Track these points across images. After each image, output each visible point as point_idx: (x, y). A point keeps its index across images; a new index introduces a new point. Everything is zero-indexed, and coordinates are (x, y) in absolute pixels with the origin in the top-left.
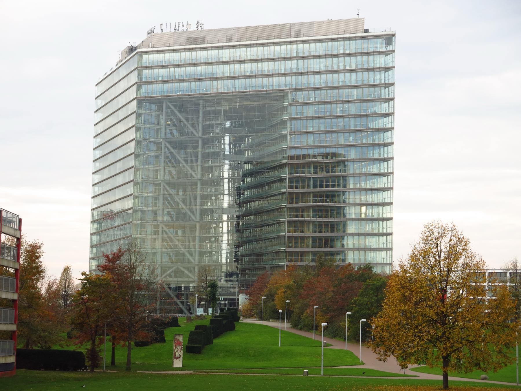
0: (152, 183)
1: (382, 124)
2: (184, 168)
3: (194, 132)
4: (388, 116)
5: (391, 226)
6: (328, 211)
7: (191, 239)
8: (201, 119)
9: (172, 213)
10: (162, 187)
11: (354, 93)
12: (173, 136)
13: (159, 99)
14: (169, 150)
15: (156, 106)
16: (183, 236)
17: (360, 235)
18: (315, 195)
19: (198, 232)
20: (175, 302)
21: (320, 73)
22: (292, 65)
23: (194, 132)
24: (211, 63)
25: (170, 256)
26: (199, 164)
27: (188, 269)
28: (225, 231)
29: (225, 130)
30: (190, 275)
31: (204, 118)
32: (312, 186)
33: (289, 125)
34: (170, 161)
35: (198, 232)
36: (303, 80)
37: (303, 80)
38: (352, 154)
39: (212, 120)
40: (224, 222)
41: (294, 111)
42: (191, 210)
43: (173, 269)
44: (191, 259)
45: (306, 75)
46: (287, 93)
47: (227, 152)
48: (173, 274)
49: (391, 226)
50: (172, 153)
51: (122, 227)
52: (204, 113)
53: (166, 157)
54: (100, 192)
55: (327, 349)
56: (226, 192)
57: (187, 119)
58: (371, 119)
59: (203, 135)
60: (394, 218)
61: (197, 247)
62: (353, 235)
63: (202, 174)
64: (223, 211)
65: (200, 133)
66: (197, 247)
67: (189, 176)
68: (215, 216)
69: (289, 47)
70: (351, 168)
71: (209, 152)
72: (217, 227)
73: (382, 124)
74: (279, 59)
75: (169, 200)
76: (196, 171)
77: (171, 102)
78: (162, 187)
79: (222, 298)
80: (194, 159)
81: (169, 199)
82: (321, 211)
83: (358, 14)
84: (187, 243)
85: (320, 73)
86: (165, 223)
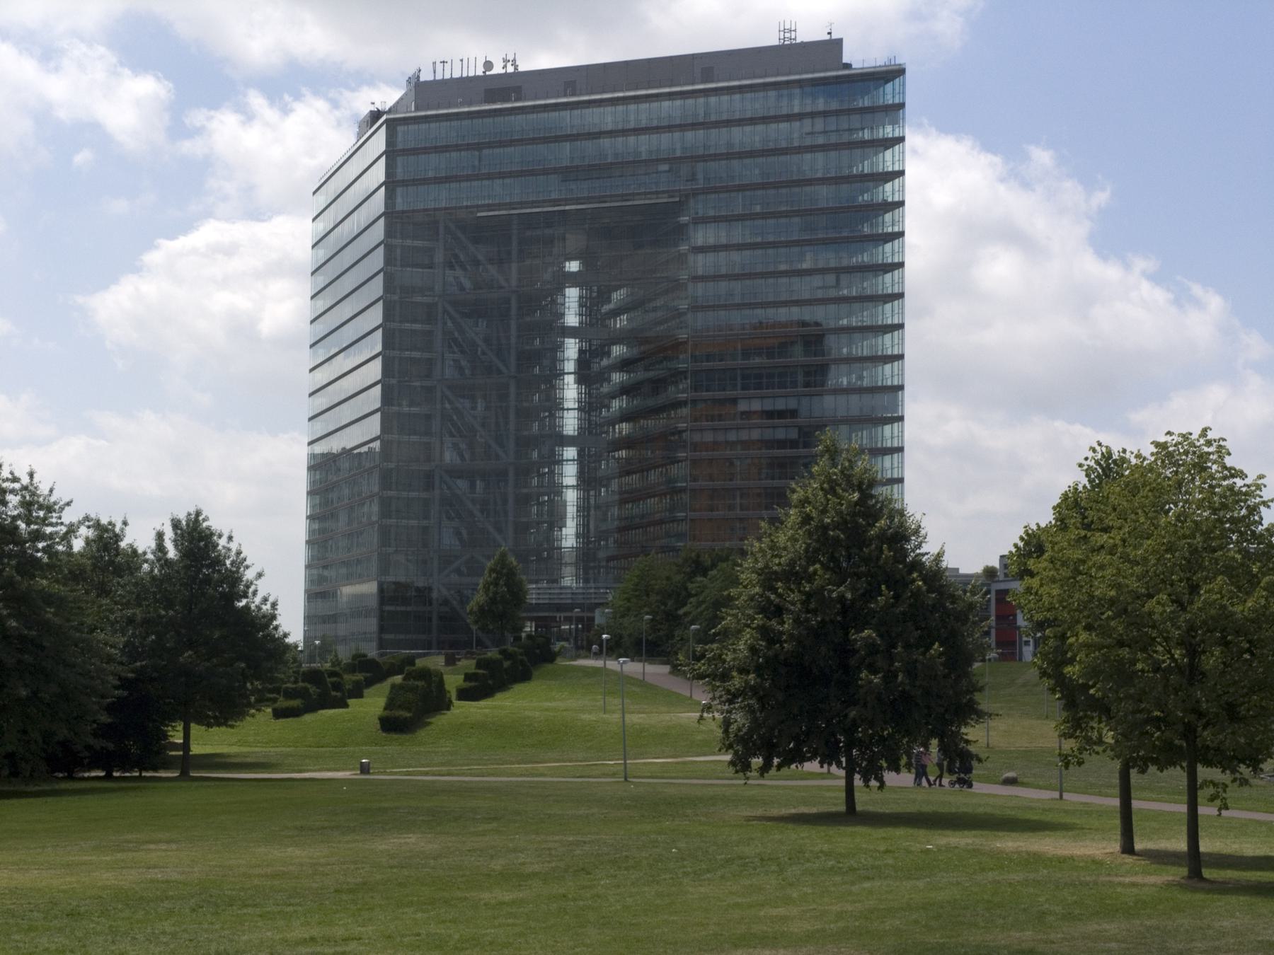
1: (880, 287)
4: (892, 270)
5: (900, 373)
21: (753, 121)
24: (534, 141)
29: (574, 280)
32: (739, 386)
41: (702, 263)
45: (724, 127)
48: (464, 569)
49: (900, 373)
54: (327, 282)
58: (858, 152)
69: (690, 102)
72: (552, 472)
73: (880, 287)
74: (670, 128)
79: (560, 618)
85: (753, 121)
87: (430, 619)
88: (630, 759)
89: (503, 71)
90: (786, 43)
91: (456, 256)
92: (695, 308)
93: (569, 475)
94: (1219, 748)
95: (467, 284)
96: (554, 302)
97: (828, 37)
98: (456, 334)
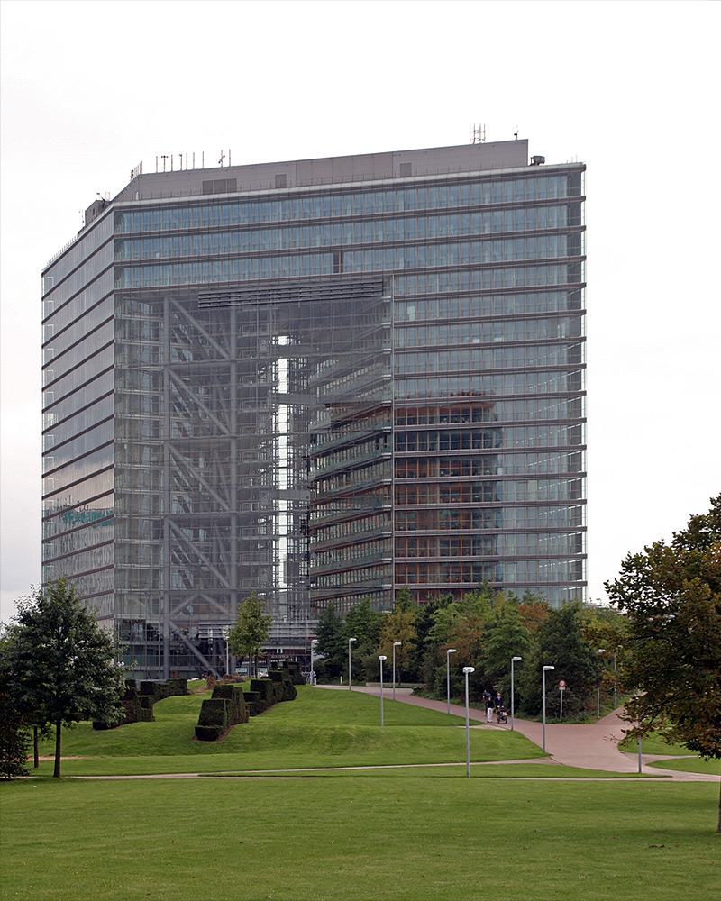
0: (148, 446)
2: (206, 417)
3: (221, 351)
6: (472, 490)
7: (221, 546)
8: (233, 327)
9: (187, 499)
10: (166, 451)
11: (512, 279)
12: (185, 360)
13: (155, 293)
14: (176, 384)
15: (150, 305)
16: (207, 541)
17: (527, 532)
18: (445, 541)
19: (233, 531)
20: (196, 657)
22: (398, 230)
23: (221, 351)
25: (185, 576)
26: (233, 333)
27: (218, 598)
28: (283, 531)
29: (283, 351)
30: (222, 609)
31: (238, 326)
33: (393, 336)
34: (179, 405)
35: (233, 531)
36: (419, 257)
37: (419, 257)
38: (508, 386)
39: (254, 330)
40: (281, 514)
41: (402, 339)
42: (219, 490)
43: (192, 598)
44: (224, 581)
46: (389, 277)
47: (283, 486)
48: (190, 609)
50: (182, 391)
51: (97, 550)
52: (238, 318)
53: (172, 398)
55: (473, 729)
56: (283, 463)
57: (208, 329)
59: (237, 357)
60: (588, 529)
61: (233, 558)
62: (513, 451)
63: (238, 582)
64: (279, 495)
65: (233, 352)
66: (233, 558)
67: (215, 431)
68: (263, 503)
70: (510, 438)
71: (249, 413)
75: (180, 551)
76: (228, 497)
77: (177, 299)
78: (166, 451)
80: (222, 400)
81: (180, 473)
82: (454, 543)
83: (516, 134)
84: (215, 553)
86: (173, 442)
87: (162, 653)
88: (70, 754)
89: (219, 166)
90: (476, 143)
91: (178, 331)
92: (398, 378)
93: (284, 523)
94: (418, 740)
95: (189, 355)
96: (268, 371)
97: (514, 138)
98: (181, 400)
